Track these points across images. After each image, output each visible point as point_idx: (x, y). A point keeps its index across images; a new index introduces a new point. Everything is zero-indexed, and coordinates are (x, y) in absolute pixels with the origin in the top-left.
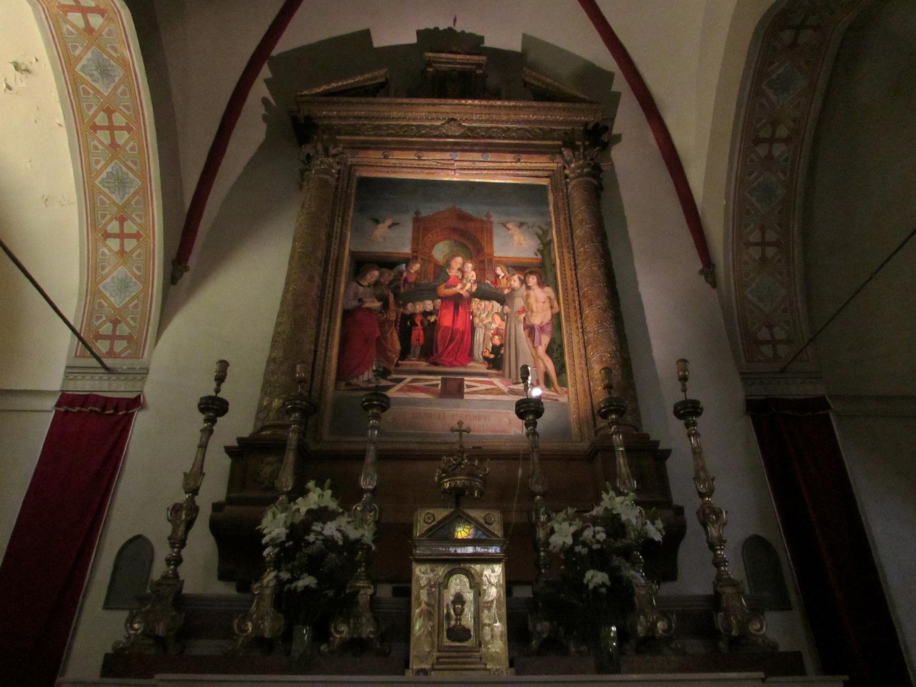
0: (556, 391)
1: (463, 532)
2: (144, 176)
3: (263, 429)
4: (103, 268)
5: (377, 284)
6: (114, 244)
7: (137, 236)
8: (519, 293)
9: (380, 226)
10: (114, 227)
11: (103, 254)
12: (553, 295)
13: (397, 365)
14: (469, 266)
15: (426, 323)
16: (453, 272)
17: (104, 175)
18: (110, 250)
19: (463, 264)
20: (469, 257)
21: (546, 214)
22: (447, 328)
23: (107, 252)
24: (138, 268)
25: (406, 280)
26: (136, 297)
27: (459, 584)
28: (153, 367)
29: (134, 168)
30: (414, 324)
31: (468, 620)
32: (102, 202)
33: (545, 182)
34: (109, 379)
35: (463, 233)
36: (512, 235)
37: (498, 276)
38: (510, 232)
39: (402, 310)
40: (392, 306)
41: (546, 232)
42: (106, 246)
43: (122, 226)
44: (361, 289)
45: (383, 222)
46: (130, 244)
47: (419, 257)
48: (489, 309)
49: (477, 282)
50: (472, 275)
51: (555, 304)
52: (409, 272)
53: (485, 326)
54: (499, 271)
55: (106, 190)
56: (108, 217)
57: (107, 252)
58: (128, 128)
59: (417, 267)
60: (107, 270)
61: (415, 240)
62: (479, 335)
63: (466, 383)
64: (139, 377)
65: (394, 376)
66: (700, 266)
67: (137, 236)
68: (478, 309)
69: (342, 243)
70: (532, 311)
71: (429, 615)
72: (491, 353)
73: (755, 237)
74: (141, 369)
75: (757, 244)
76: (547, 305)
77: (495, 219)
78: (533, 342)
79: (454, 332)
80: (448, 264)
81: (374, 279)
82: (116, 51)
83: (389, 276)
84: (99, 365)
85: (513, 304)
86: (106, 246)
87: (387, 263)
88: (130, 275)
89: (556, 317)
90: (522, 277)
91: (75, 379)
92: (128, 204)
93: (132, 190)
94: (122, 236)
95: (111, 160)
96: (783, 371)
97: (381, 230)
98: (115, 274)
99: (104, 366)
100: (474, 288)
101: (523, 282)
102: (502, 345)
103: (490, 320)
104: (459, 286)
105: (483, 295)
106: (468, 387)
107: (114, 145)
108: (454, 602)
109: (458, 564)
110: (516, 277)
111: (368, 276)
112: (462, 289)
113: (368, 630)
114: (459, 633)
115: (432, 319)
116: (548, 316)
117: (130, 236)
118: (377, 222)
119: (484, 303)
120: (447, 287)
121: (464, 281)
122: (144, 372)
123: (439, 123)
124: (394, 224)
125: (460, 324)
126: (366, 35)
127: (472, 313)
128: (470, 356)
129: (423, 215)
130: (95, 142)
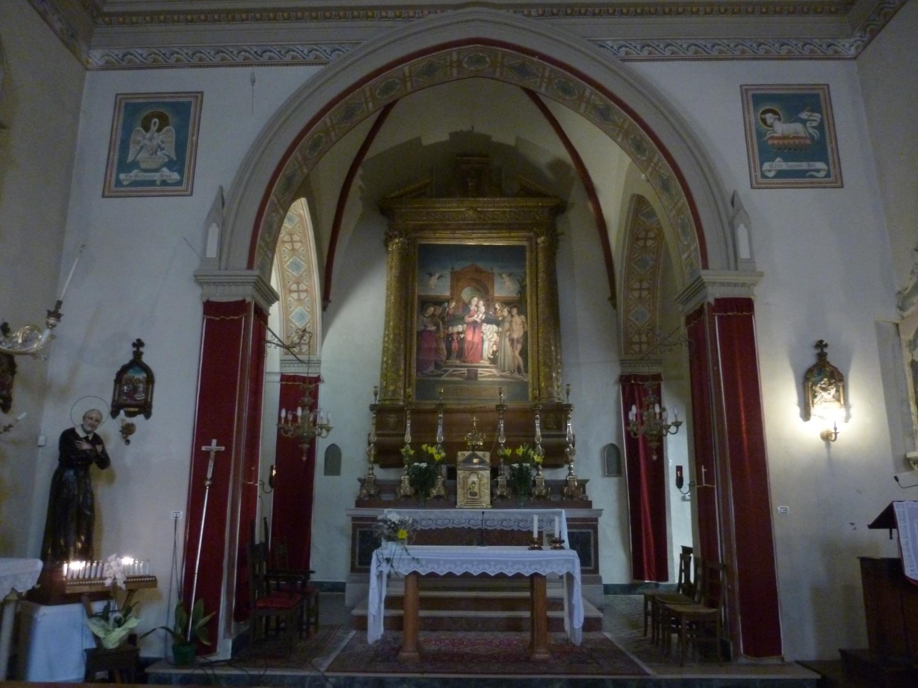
0: (523, 376)
1: (475, 461)
2: (308, 262)
3: (385, 400)
4: (290, 307)
5: (433, 315)
6: (295, 295)
7: (306, 291)
8: (507, 320)
9: (433, 278)
10: (294, 287)
11: (290, 301)
12: (524, 320)
13: (445, 363)
14: (481, 303)
15: (459, 339)
16: (473, 308)
17: (288, 263)
18: (293, 298)
19: (478, 302)
20: (481, 298)
21: (524, 267)
22: (470, 341)
23: (292, 300)
24: (308, 307)
25: (448, 314)
26: (309, 322)
27: (474, 478)
28: (323, 359)
29: (304, 259)
30: (453, 339)
31: (476, 490)
32: (288, 276)
33: (525, 243)
34: (302, 366)
35: (478, 281)
36: (504, 283)
37: (496, 309)
38: (503, 280)
39: (446, 331)
40: (442, 329)
41: (524, 279)
42: (291, 297)
43: (298, 286)
44: (425, 319)
45: (434, 275)
46: (303, 295)
47: (455, 298)
48: (491, 329)
49: (485, 313)
50: (483, 309)
51: (526, 326)
52: (449, 308)
53: (489, 339)
54: (497, 306)
55: (290, 270)
56: (291, 283)
57: (292, 300)
58: (300, 241)
59: (453, 304)
60: (292, 308)
61: (452, 287)
62: (486, 346)
63: (479, 372)
64: (317, 365)
65: (444, 369)
66: (609, 295)
67: (306, 291)
68: (485, 330)
69: (413, 292)
70: (513, 331)
71: (463, 488)
72: (492, 355)
73: (637, 285)
74: (317, 361)
75: (638, 290)
76: (521, 327)
77: (496, 270)
78: (513, 348)
79: (473, 343)
80: (470, 303)
81: (431, 313)
82: (296, 211)
83: (439, 310)
84: (295, 359)
85: (504, 326)
86: (291, 297)
87: (438, 302)
88: (305, 311)
89: (525, 333)
90: (509, 309)
91: (285, 366)
92: (301, 275)
93: (303, 270)
94: (298, 291)
95: (292, 256)
96: (642, 359)
97: (434, 281)
98: (297, 310)
99: (298, 360)
100: (484, 317)
101: (510, 312)
102: (497, 351)
103: (491, 336)
104: (476, 316)
105: (488, 321)
106: (480, 374)
107: (293, 249)
108: (472, 484)
109: (474, 471)
110: (506, 310)
111: (428, 311)
112: (477, 317)
113: (443, 492)
114: (474, 494)
115: (462, 336)
116: (522, 333)
117: (303, 291)
118: (431, 275)
119: (489, 326)
120: (470, 317)
121: (479, 313)
122: (319, 362)
123: (464, 209)
124: (440, 277)
125: (476, 340)
126: (418, 139)
127: (482, 332)
128: (481, 357)
129: (457, 270)
130: (284, 249)
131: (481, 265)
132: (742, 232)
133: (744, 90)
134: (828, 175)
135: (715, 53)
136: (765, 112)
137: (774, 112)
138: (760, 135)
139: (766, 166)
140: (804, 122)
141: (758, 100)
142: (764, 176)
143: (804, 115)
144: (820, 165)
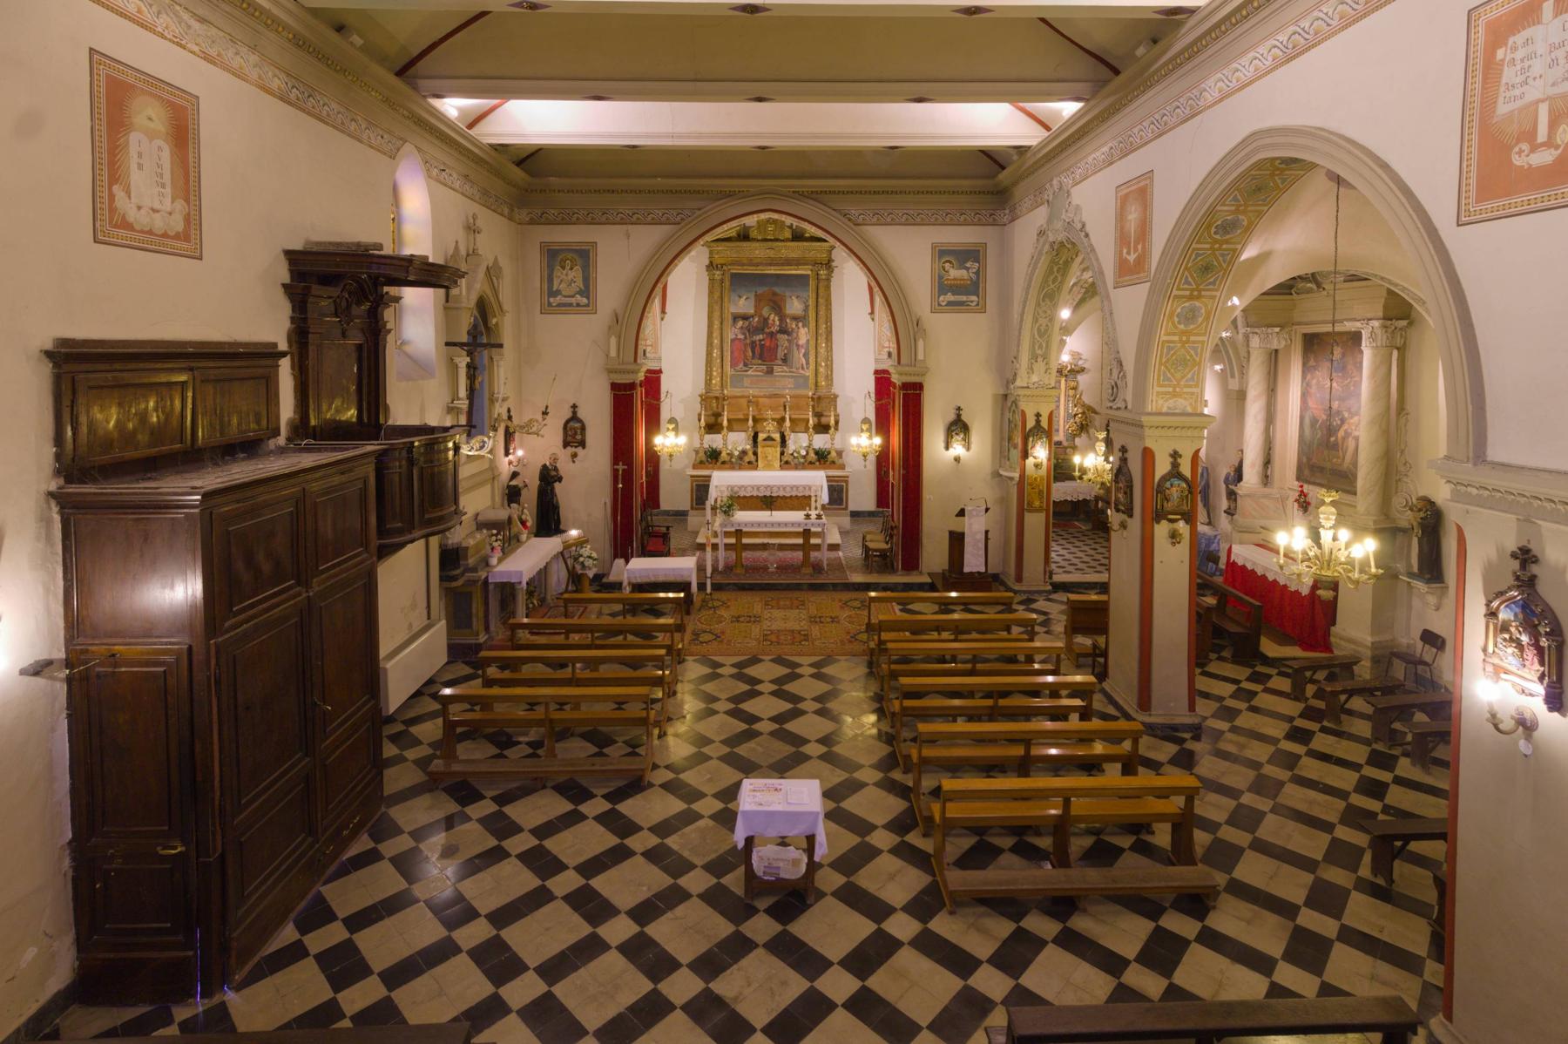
14: (777, 318)
16: (770, 322)
20: (776, 314)
21: (808, 291)
33: (809, 272)
50: (777, 323)
61: (756, 306)
131: (777, 290)
132: (921, 343)
133: (934, 247)
134: (978, 305)
135: (918, 220)
136: (947, 261)
137: (950, 262)
138: (940, 277)
139: (942, 298)
140: (967, 269)
141: (942, 253)
142: (939, 305)
143: (968, 265)
144: (974, 298)
